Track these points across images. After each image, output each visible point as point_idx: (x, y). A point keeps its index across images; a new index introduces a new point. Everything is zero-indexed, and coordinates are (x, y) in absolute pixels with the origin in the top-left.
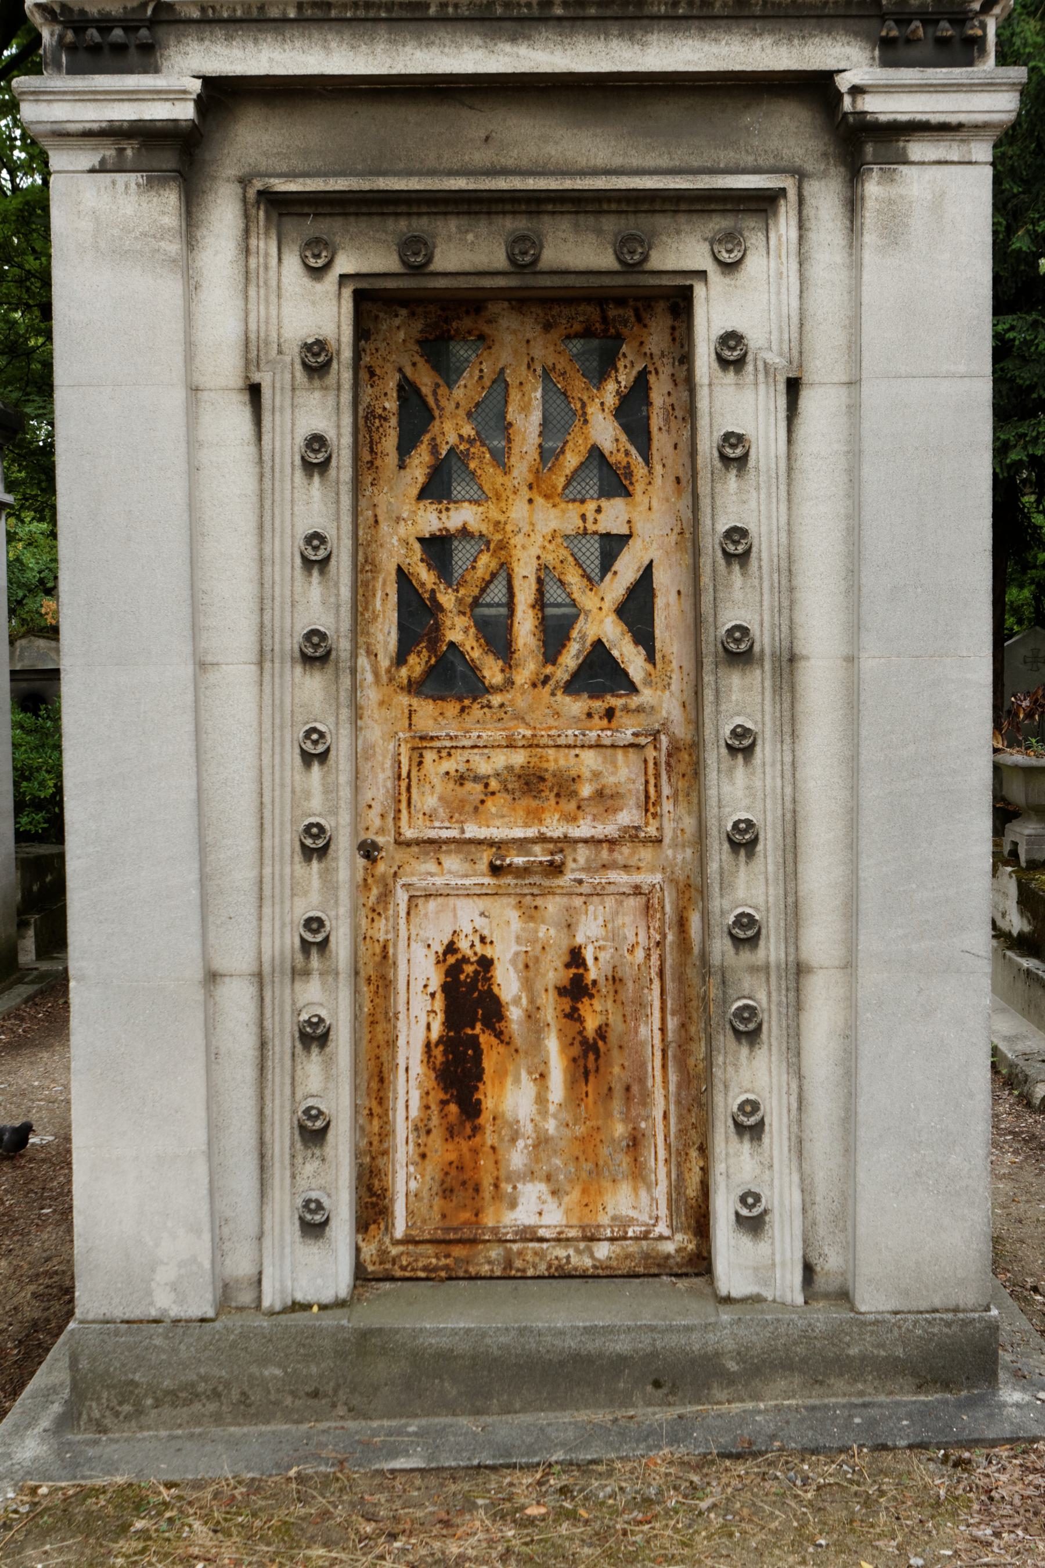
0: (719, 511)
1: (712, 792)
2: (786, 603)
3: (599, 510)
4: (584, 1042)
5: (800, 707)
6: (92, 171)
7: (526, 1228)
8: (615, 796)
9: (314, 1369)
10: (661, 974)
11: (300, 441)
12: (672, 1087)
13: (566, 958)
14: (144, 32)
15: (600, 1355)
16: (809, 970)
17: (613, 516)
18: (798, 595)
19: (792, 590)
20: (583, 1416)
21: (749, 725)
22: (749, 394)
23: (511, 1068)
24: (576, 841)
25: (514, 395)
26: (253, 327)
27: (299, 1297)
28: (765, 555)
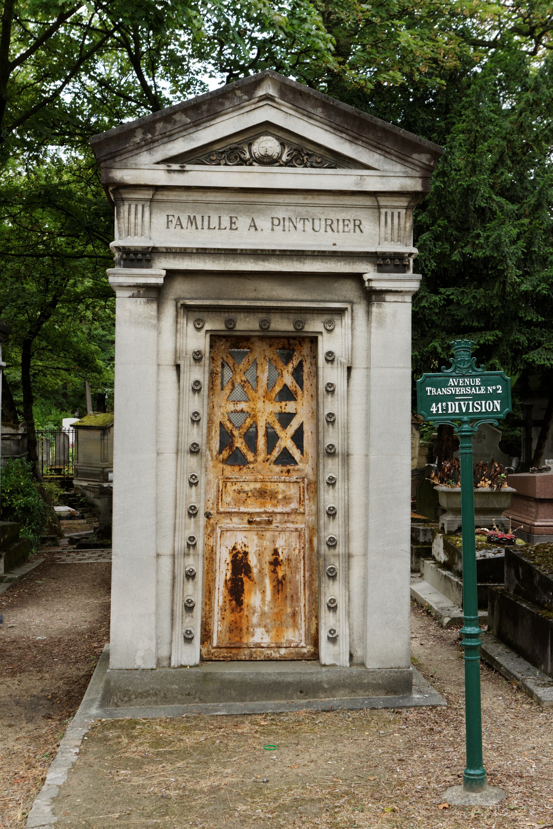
0: (325, 407)
1: (322, 498)
2: (346, 437)
3: (286, 405)
4: (278, 580)
5: (350, 471)
6: (130, 297)
7: (257, 643)
8: (290, 498)
9: (188, 686)
10: (304, 558)
11: (192, 382)
12: (307, 596)
13: (272, 552)
14: (148, 256)
15: (283, 682)
16: (353, 556)
17: (290, 407)
18: (350, 435)
19: (348, 433)
20: (277, 702)
21: (334, 476)
22: (335, 371)
23: (253, 589)
24: (277, 513)
25: (260, 367)
26: (178, 346)
27: (183, 663)
28: (340, 422)
